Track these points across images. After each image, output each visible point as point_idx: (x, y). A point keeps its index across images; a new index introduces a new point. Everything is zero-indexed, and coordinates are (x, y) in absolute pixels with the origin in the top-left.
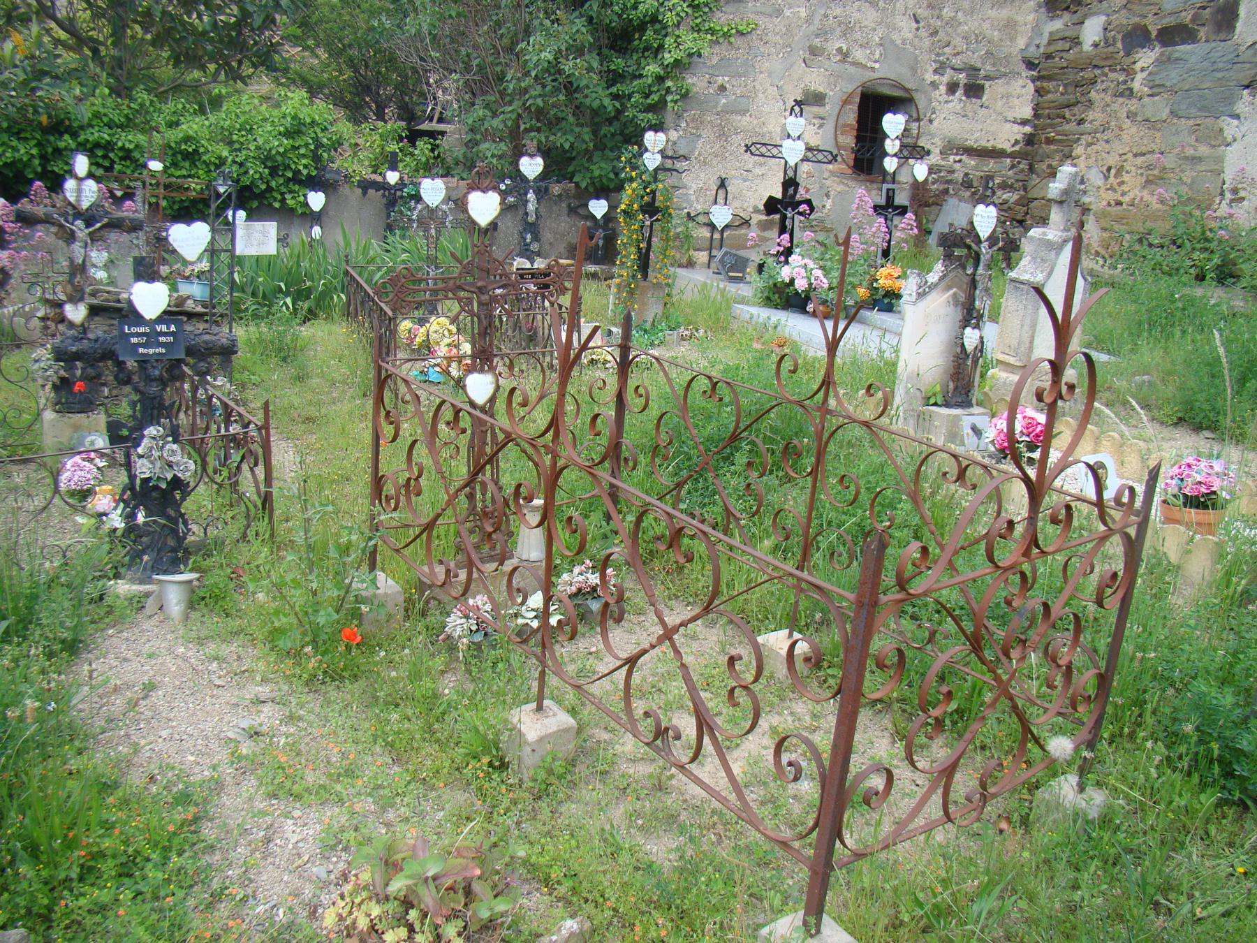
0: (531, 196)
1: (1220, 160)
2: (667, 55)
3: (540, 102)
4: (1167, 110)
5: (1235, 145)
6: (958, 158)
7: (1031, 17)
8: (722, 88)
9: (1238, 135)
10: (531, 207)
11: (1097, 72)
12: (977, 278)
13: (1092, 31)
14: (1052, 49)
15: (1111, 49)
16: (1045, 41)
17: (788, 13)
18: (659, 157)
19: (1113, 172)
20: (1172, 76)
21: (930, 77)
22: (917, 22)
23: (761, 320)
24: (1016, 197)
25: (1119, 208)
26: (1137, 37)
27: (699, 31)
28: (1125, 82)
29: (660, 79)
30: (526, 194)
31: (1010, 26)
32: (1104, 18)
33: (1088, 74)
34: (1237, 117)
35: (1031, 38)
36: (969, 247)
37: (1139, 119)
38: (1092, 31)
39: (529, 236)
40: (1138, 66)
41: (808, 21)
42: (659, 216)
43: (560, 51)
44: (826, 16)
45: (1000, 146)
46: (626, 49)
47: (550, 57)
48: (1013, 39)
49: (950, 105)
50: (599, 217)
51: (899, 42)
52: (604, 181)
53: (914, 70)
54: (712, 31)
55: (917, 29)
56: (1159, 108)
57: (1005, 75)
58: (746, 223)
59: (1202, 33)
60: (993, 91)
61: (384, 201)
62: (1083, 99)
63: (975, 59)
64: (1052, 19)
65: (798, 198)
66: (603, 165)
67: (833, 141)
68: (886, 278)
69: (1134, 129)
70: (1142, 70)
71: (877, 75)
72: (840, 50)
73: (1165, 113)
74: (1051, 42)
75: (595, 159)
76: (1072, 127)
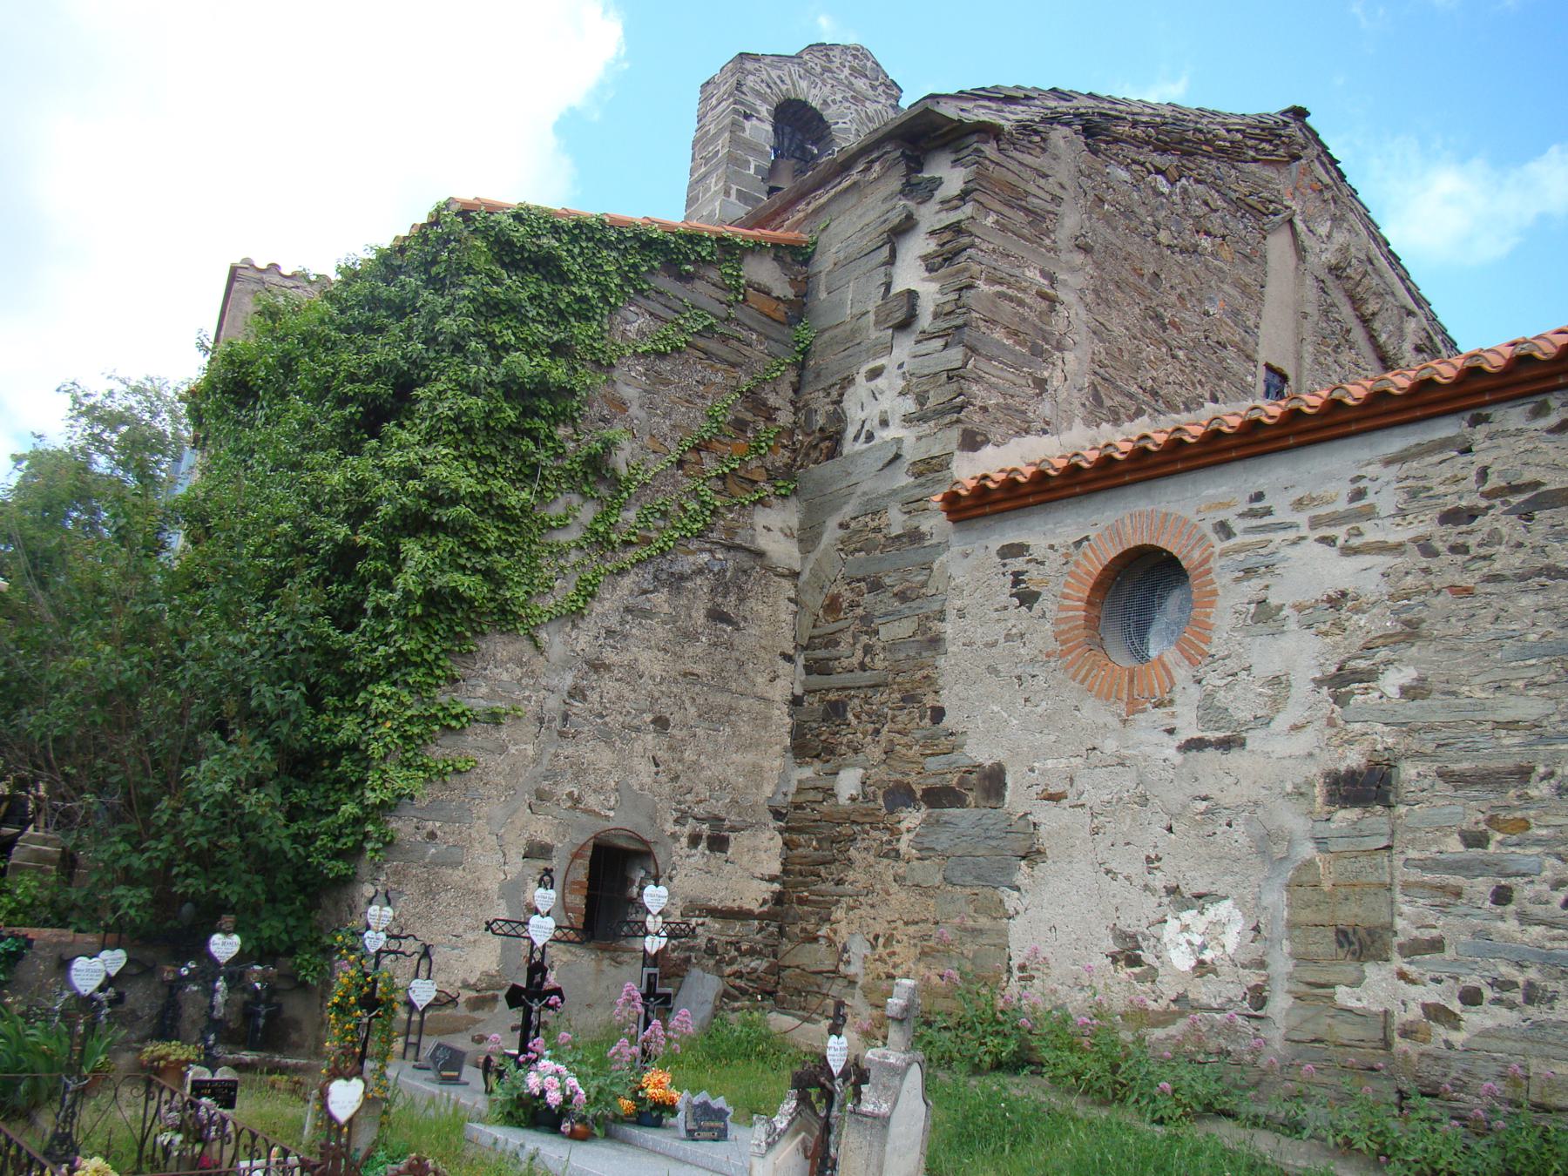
0: (220, 984)
1: (1003, 933)
2: (368, 794)
3: (203, 841)
4: (940, 877)
5: (1018, 918)
6: (700, 921)
7: (777, 763)
9: (1021, 909)
10: (219, 999)
11: (857, 828)
12: (832, 1121)
13: (848, 783)
14: (801, 799)
15: (871, 805)
16: (793, 789)
18: (383, 936)
19: (881, 940)
20: (942, 840)
21: (670, 827)
22: (657, 765)
23: (510, 1147)
24: (765, 964)
26: (900, 796)
27: (409, 767)
28: (889, 842)
29: (357, 821)
30: (215, 981)
31: (756, 773)
33: (846, 830)
34: (1018, 889)
35: (777, 785)
36: (823, 1086)
38: (848, 783)
39: (212, 1037)
40: (903, 826)
41: (536, 761)
42: (380, 1011)
43: (238, 781)
45: (746, 907)
46: (309, 775)
47: (227, 789)
48: (758, 786)
49: (692, 860)
51: (636, 787)
52: (274, 943)
53: (652, 819)
54: (424, 767)
55: (657, 773)
56: (930, 873)
57: (752, 826)
58: (453, 1001)
60: (738, 842)
62: (840, 857)
63: (718, 808)
64: (800, 765)
65: (546, 986)
66: (274, 923)
68: (656, 1086)
69: (903, 895)
70: (908, 830)
71: (612, 825)
72: (570, 795)
73: (938, 879)
74: (799, 791)
75: (264, 915)
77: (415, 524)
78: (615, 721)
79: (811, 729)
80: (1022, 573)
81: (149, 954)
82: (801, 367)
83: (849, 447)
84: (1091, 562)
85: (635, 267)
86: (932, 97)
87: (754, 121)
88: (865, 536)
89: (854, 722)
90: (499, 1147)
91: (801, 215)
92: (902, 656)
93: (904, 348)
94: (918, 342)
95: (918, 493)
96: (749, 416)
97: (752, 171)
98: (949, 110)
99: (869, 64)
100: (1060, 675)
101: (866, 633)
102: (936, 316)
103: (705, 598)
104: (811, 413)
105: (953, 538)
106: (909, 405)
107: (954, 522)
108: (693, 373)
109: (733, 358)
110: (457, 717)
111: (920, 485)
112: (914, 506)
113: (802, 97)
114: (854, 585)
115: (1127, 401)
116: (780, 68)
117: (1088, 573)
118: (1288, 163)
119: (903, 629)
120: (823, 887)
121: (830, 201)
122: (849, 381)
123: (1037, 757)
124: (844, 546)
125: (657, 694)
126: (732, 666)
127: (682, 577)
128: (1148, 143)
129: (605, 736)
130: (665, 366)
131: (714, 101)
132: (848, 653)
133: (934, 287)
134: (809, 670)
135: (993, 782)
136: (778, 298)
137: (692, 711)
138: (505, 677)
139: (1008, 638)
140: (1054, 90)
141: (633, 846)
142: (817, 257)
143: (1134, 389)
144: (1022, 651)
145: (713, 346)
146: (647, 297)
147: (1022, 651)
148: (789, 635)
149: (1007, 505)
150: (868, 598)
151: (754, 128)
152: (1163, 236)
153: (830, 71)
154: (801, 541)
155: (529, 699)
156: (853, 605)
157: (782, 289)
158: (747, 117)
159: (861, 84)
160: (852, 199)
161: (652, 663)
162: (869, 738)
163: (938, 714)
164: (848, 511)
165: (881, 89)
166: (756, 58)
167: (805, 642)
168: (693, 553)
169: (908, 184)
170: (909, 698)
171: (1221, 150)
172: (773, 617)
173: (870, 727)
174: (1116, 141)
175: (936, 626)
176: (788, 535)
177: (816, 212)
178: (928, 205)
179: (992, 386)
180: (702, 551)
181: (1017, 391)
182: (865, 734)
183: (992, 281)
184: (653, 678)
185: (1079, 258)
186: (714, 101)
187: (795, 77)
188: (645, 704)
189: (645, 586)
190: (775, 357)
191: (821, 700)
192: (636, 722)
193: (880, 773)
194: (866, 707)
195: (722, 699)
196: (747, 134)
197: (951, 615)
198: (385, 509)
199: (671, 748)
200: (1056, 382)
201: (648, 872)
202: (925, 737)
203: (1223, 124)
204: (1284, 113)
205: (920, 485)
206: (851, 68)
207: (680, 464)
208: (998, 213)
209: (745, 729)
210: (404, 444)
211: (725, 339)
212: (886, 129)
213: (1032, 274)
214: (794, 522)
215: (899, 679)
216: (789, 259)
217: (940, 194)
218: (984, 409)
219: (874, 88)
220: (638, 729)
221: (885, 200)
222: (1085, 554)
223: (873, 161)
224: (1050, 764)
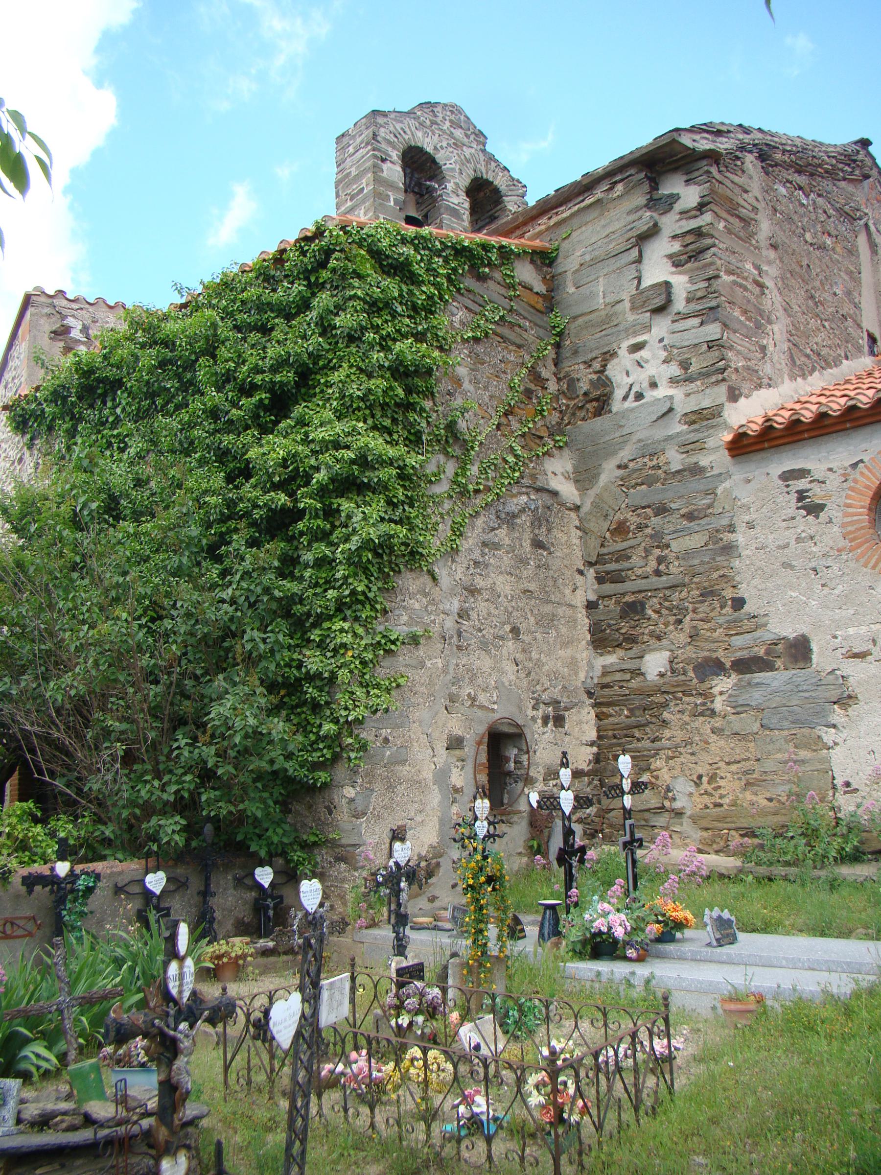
4: (758, 725)
5: (837, 748)
8: (386, 740)
13: (655, 663)
16: (599, 673)
17: (428, 664)
18: (485, 823)
19: (705, 779)
21: (530, 713)
22: (517, 665)
25: (718, 809)
28: (704, 704)
31: (573, 664)
32: (668, 653)
33: (659, 699)
34: (834, 726)
35: (587, 672)
37: (726, 733)
38: (655, 663)
41: (445, 671)
44: (457, 665)
48: (576, 674)
49: (546, 736)
50: (266, 885)
51: (507, 684)
59: (779, 663)
61: (53, 897)
63: (555, 693)
67: (473, 781)
69: (722, 743)
70: (721, 693)
71: (497, 716)
72: (469, 695)
73: (756, 727)
74: (604, 674)
76: (646, 744)
77: (348, 485)
78: (488, 633)
79: (609, 626)
80: (807, 491)
81: (180, 871)
82: (558, 346)
83: (617, 405)
84: (869, 479)
85: (454, 270)
86: (677, 130)
87: (388, 164)
88: (644, 473)
89: (654, 616)
90: (604, 979)
91: (543, 227)
92: (696, 562)
93: (661, 327)
94: (673, 322)
95: (693, 437)
96: (532, 386)
97: (392, 203)
98: (686, 140)
99: (462, 118)
100: (852, 564)
101: (658, 547)
102: (689, 301)
103: (528, 530)
104: (572, 383)
105: (732, 469)
106: (674, 370)
107: (733, 456)
108: (496, 354)
109: (518, 341)
110: (393, 642)
111: (694, 431)
112: (689, 447)
113: (419, 145)
114: (639, 511)
115: (808, 362)
116: (402, 122)
117: (867, 487)
118: (861, 181)
119: (695, 541)
120: (639, 745)
121: (573, 215)
122: (614, 355)
123: (838, 628)
124: (625, 483)
125: (510, 609)
126: (550, 583)
127: (514, 516)
128: (791, 167)
129: (484, 646)
130: (480, 349)
131: (351, 150)
132: (642, 563)
133: (684, 279)
134: (600, 580)
135: (799, 650)
136: (537, 293)
137: (532, 619)
138: (417, 606)
139: (798, 540)
140: (740, 126)
141: (512, 730)
142: (559, 260)
143: (808, 351)
144: (814, 549)
145: (505, 331)
146: (462, 295)
147: (814, 549)
148: (579, 554)
149: (786, 440)
150: (655, 520)
151: (389, 169)
152: (808, 236)
153: (436, 123)
154: (576, 481)
155: (434, 622)
156: (640, 527)
157: (539, 287)
158: (383, 160)
159: (458, 133)
160: (594, 214)
161: (504, 585)
162: (671, 627)
163: (739, 603)
164: (625, 455)
165: (472, 137)
166: (384, 114)
167: (593, 559)
168: (515, 496)
169: (651, 200)
170: (708, 593)
171: (827, 172)
172: (570, 543)
173: (672, 619)
174: (776, 165)
175: (727, 537)
176: (568, 478)
177: (558, 224)
178: (668, 215)
179: (739, 353)
180: (521, 494)
181: (751, 355)
182: (666, 625)
183: (730, 273)
184: (506, 596)
185: (772, 254)
186: (351, 150)
187: (413, 129)
188: (504, 617)
189: (492, 524)
190: (542, 339)
191: (617, 602)
192: (501, 633)
193: (690, 652)
194: (667, 604)
195: (547, 609)
196: (385, 174)
197: (741, 527)
198: (321, 476)
199: (524, 651)
200: (771, 348)
201: (520, 750)
202: (728, 621)
203: (826, 152)
204: (856, 143)
205: (694, 431)
206: (451, 121)
207: (498, 427)
208: (726, 220)
209: (564, 630)
210: (322, 421)
211: (512, 325)
212: (632, 157)
213: (749, 266)
214: (569, 467)
215: (695, 580)
216: (539, 262)
217: (678, 207)
218: (736, 370)
219: (468, 136)
220: (502, 638)
221: (629, 213)
222: (862, 473)
223: (616, 183)
224: (851, 631)
